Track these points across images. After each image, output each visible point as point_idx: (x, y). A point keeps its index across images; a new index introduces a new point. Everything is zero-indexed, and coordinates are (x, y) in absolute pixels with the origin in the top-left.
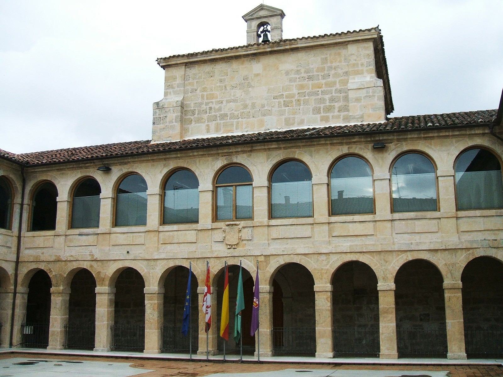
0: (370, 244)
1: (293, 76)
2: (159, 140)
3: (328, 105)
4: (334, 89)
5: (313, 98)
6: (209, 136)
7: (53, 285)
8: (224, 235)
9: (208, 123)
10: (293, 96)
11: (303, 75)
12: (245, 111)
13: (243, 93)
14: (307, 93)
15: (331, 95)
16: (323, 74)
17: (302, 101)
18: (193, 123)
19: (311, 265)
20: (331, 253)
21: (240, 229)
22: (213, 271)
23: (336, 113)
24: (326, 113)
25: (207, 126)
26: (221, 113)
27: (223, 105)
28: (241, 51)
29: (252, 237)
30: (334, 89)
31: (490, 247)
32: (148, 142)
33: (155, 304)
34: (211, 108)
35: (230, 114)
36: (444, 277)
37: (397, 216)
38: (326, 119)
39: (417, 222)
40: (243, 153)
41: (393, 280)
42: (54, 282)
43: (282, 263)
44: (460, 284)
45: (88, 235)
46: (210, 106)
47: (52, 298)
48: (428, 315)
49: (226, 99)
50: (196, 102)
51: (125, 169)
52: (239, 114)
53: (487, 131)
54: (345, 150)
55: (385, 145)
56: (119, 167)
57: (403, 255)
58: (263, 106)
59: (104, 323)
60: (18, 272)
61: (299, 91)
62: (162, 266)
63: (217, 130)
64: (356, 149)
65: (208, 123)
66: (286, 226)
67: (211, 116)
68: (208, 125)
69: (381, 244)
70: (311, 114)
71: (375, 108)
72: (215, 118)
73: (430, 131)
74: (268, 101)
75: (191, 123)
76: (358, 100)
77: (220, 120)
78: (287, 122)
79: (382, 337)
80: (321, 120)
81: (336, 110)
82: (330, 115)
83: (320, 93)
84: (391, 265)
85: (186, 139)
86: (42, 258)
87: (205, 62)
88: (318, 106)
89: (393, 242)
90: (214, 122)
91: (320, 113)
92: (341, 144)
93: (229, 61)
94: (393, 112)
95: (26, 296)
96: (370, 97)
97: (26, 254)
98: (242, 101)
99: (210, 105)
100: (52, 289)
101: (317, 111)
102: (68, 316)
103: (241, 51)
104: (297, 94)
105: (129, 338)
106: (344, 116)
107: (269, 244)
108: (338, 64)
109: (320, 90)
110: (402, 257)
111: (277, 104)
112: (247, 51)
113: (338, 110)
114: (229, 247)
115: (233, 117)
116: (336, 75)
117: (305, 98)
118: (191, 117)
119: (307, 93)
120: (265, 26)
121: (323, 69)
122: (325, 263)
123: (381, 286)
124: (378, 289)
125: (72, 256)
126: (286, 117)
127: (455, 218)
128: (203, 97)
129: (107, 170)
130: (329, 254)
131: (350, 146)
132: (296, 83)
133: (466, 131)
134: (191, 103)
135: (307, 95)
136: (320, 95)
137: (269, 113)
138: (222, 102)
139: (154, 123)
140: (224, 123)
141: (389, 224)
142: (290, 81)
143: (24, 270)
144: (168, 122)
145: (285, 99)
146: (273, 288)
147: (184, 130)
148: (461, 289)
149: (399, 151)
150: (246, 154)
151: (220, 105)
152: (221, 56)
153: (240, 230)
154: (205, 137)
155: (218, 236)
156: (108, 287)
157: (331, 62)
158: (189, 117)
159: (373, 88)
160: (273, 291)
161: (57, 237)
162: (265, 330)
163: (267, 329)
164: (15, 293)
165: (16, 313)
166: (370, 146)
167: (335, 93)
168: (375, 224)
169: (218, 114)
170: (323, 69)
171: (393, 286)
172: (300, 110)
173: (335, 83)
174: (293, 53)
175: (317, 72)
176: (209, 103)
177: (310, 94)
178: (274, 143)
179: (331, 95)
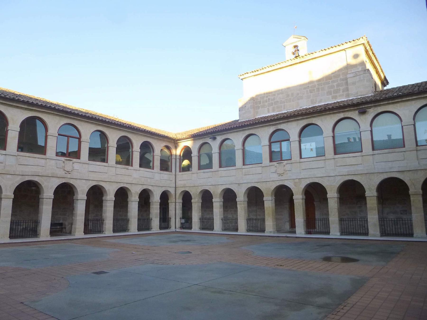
4: (339, 79)
6: (269, 115)
8: (276, 169)
15: (337, 83)
18: (260, 109)
19: (325, 183)
30: (339, 79)
32: (238, 120)
34: (269, 99)
36: (410, 187)
38: (335, 97)
39: (389, 155)
41: (375, 190)
42: (193, 197)
43: (309, 182)
47: (193, 205)
48: (406, 211)
51: (224, 137)
54: (342, 115)
55: (366, 110)
56: (220, 136)
58: (298, 94)
75: (259, 109)
78: (312, 102)
79: (369, 224)
80: (332, 98)
81: (341, 91)
82: (338, 94)
85: (257, 117)
86: (187, 185)
88: (330, 90)
89: (374, 168)
90: (271, 106)
92: (339, 112)
94: (388, 85)
95: (181, 204)
97: (179, 183)
99: (269, 97)
100: (193, 201)
101: (329, 93)
102: (201, 214)
104: (317, 85)
105: (311, 230)
107: (300, 172)
114: (279, 175)
117: (322, 86)
118: (259, 105)
124: (366, 195)
125: (200, 184)
127: (416, 151)
129: (214, 139)
141: (371, 157)
143: (179, 191)
146: (339, 195)
149: (376, 113)
154: (267, 115)
155: (273, 169)
156: (219, 198)
159: (363, 75)
164: (176, 203)
165: (176, 212)
166: (357, 112)
167: (340, 81)
168: (325, 161)
169: (273, 102)
171: (375, 194)
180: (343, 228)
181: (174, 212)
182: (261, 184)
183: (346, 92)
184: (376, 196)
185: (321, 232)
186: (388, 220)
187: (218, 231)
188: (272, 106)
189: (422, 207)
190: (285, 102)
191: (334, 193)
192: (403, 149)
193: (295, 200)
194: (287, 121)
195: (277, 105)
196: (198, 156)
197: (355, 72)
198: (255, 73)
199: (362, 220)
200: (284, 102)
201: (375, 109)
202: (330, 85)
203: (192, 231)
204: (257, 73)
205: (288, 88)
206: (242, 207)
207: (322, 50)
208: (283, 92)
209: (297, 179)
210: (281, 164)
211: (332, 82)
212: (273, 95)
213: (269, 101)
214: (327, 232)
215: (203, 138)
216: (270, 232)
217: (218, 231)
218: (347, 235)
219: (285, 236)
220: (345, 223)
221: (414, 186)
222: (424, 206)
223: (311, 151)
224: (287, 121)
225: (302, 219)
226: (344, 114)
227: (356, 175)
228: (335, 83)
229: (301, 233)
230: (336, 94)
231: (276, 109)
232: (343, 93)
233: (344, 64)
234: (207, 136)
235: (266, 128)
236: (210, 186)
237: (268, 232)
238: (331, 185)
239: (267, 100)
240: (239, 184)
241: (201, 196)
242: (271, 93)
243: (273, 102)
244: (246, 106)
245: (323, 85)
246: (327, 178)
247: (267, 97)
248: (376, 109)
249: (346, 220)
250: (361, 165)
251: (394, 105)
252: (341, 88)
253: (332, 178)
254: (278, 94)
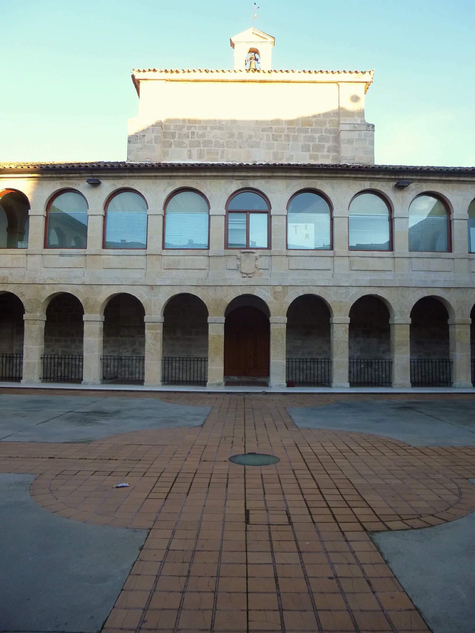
0: (387, 278)
4: (324, 128)
5: (303, 135)
7: (27, 311)
9: (190, 149)
10: (282, 130)
12: (231, 140)
14: (296, 129)
15: (321, 134)
17: (291, 137)
18: (173, 147)
19: (330, 298)
21: (257, 258)
22: (226, 300)
24: (315, 152)
26: (205, 139)
34: (193, 133)
35: (215, 141)
37: (415, 254)
39: (432, 261)
41: (409, 315)
42: (26, 307)
43: (302, 294)
44: (470, 320)
45: (71, 255)
47: (26, 325)
49: (210, 125)
50: (177, 124)
52: (225, 142)
58: (250, 137)
59: (95, 353)
61: (289, 127)
63: (200, 156)
66: (304, 257)
67: (193, 141)
68: (190, 151)
72: (198, 144)
74: (256, 132)
76: (350, 142)
77: (204, 147)
81: (326, 150)
82: (320, 154)
83: (310, 131)
86: (10, 280)
90: (197, 148)
92: (364, 179)
99: (193, 129)
100: (25, 316)
101: (306, 148)
104: (286, 129)
109: (310, 128)
113: (327, 150)
115: (217, 144)
118: (171, 140)
119: (296, 129)
123: (398, 320)
125: (52, 279)
129: (95, 184)
130: (348, 287)
134: (171, 125)
135: (297, 131)
136: (310, 133)
137: (256, 145)
138: (206, 128)
140: (208, 150)
141: (407, 261)
145: (273, 133)
146: (163, 318)
148: (470, 325)
151: (204, 131)
153: (257, 259)
158: (169, 140)
160: (411, 323)
162: (282, 361)
163: (283, 360)
167: (325, 133)
172: (290, 145)
176: (191, 127)
177: (299, 130)
180: (166, 375)
182: (203, 289)
183: (333, 152)
184: (410, 324)
185: (12, 377)
187: (94, 384)
191: (345, 316)
194: (270, 174)
196: (46, 218)
197: (354, 124)
198: (169, 76)
202: (308, 135)
203: (23, 384)
204: (174, 76)
205: (234, 122)
206: (157, 333)
207: (304, 71)
209: (280, 287)
210: (250, 254)
214: (318, 382)
215: (66, 177)
216: (219, 385)
217: (94, 384)
218: (58, 381)
219: (261, 391)
220: (319, 366)
222: (472, 343)
223: (306, 238)
224: (270, 174)
226: (370, 184)
227: (382, 288)
229: (280, 385)
233: (333, 107)
234: (78, 175)
235: (223, 181)
236: (76, 286)
237: (212, 385)
238: (341, 302)
239: (188, 133)
240: (152, 287)
241: (46, 307)
242: (200, 122)
243: (201, 140)
244: (144, 136)
245: (296, 131)
246: (335, 288)
247: (189, 128)
248: (420, 185)
249: (321, 362)
250: (389, 273)
251: (445, 184)
252: (327, 145)
253: (343, 290)
254: (213, 128)
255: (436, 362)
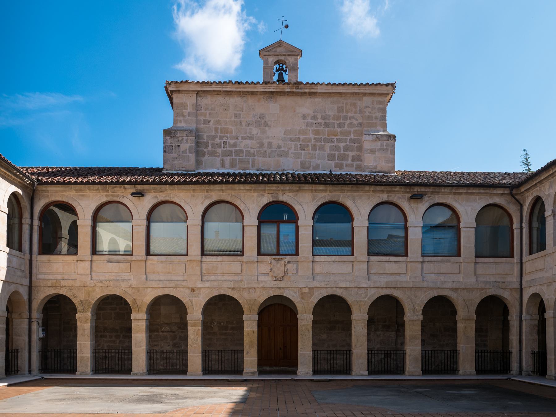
1: (310, 120)
2: (171, 169)
3: (343, 153)
5: (329, 145)
7: (79, 311)
10: (310, 140)
11: (320, 121)
13: (259, 131)
15: (345, 144)
16: (338, 122)
18: (207, 156)
20: (369, 287)
23: (350, 162)
25: (221, 160)
27: (238, 141)
28: (259, 87)
29: (297, 271)
31: (500, 288)
32: (162, 169)
33: (199, 330)
34: (225, 143)
38: (340, 166)
40: (290, 192)
41: (421, 312)
46: (224, 141)
49: (241, 135)
51: (161, 197)
53: (506, 192)
54: (385, 197)
57: (430, 291)
58: (279, 147)
60: (33, 297)
61: (316, 137)
62: (205, 294)
64: (395, 198)
65: (223, 158)
68: (222, 160)
69: (413, 282)
70: (326, 160)
71: (388, 161)
73: (461, 188)
74: (285, 142)
81: (350, 159)
83: (336, 140)
84: (420, 299)
87: (218, 93)
91: (335, 160)
92: (383, 192)
93: (244, 97)
96: (384, 150)
98: (258, 140)
100: (78, 316)
101: (331, 157)
102: (95, 342)
103: (259, 87)
104: (313, 139)
105: (162, 368)
106: (356, 165)
108: (353, 115)
109: (335, 138)
110: (429, 293)
111: (293, 146)
112: (266, 88)
116: (351, 125)
120: (281, 65)
121: (338, 118)
122: (363, 296)
126: (302, 160)
128: (216, 129)
131: (390, 194)
132: (312, 128)
133: (490, 190)
137: (285, 154)
139: (165, 151)
140: (239, 159)
142: (307, 126)
143: (40, 297)
144: (181, 152)
145: (301, 143)
147: (198, 163)
150: (292, 193)
152: (238, 90)
157: (347, 112)
161: (81, 262)
169: (233, 149)
170: (338, 118)
173: (349, 133)
174: (310, 98)
175: (332, 120)
178: (322, 185)
179: (345, 144)
181: (26, 338)
186: (380, 352)
188: (230, 156)
189: (474, 336)
190: (256, 154)
191: (364, 313)
192: (351, 258)
193: (246, 321)
195: (239, 157)
199: (378, 353)
200: (254, 154)
201: (431, 197)
208: (252, 136)
211: (337, 140)
212: (234, 137)
213: (226, 146)
216: (253, 373)
217: (142, 375)
221: (468, 309)
225: (310, 352)
228: (342, 143)
230: (342, 162)
231: (238, 164)
232: (352, 161)
237: (247, 373)
245: (322, 141)
252: (351, 154)
255: (432, 353)
